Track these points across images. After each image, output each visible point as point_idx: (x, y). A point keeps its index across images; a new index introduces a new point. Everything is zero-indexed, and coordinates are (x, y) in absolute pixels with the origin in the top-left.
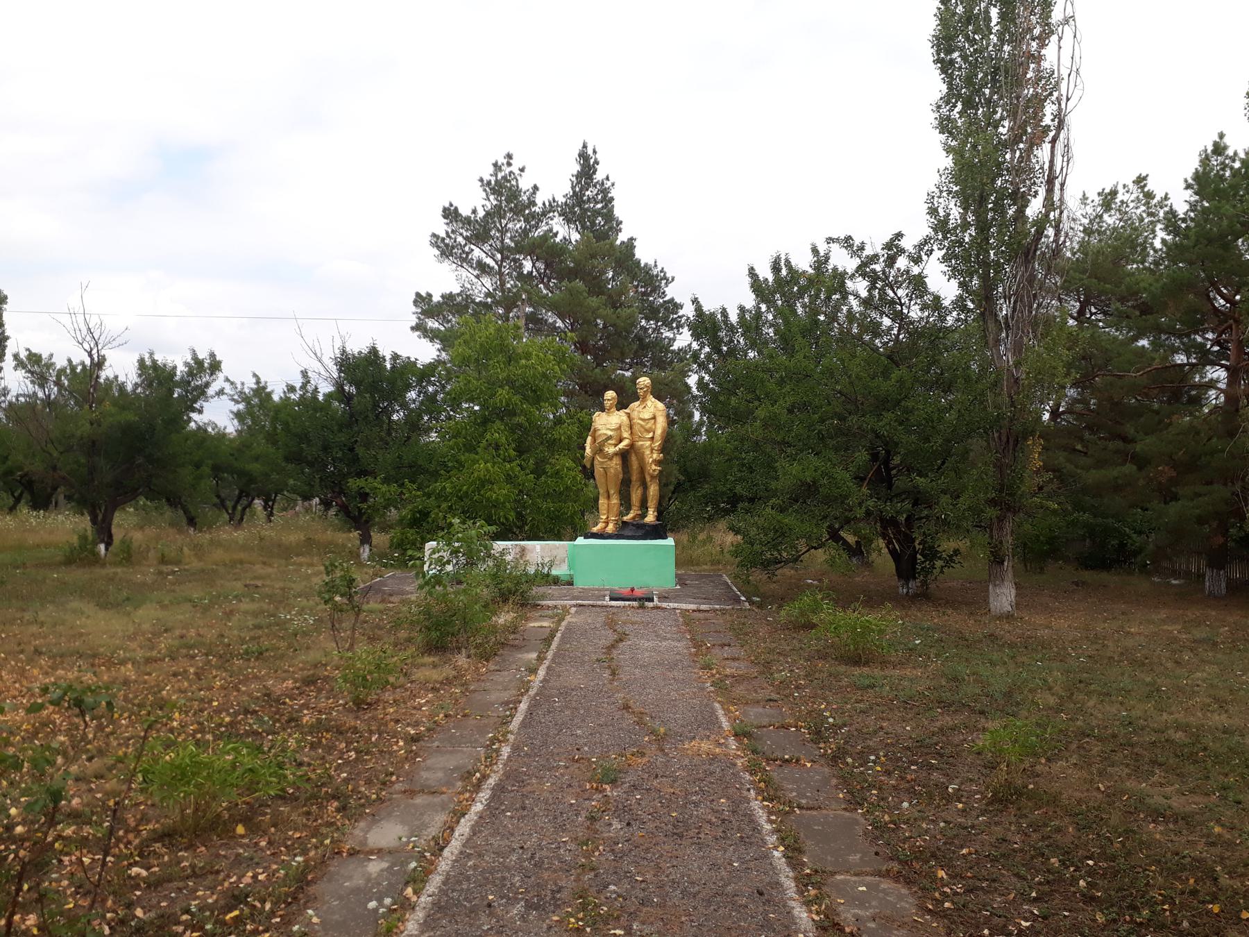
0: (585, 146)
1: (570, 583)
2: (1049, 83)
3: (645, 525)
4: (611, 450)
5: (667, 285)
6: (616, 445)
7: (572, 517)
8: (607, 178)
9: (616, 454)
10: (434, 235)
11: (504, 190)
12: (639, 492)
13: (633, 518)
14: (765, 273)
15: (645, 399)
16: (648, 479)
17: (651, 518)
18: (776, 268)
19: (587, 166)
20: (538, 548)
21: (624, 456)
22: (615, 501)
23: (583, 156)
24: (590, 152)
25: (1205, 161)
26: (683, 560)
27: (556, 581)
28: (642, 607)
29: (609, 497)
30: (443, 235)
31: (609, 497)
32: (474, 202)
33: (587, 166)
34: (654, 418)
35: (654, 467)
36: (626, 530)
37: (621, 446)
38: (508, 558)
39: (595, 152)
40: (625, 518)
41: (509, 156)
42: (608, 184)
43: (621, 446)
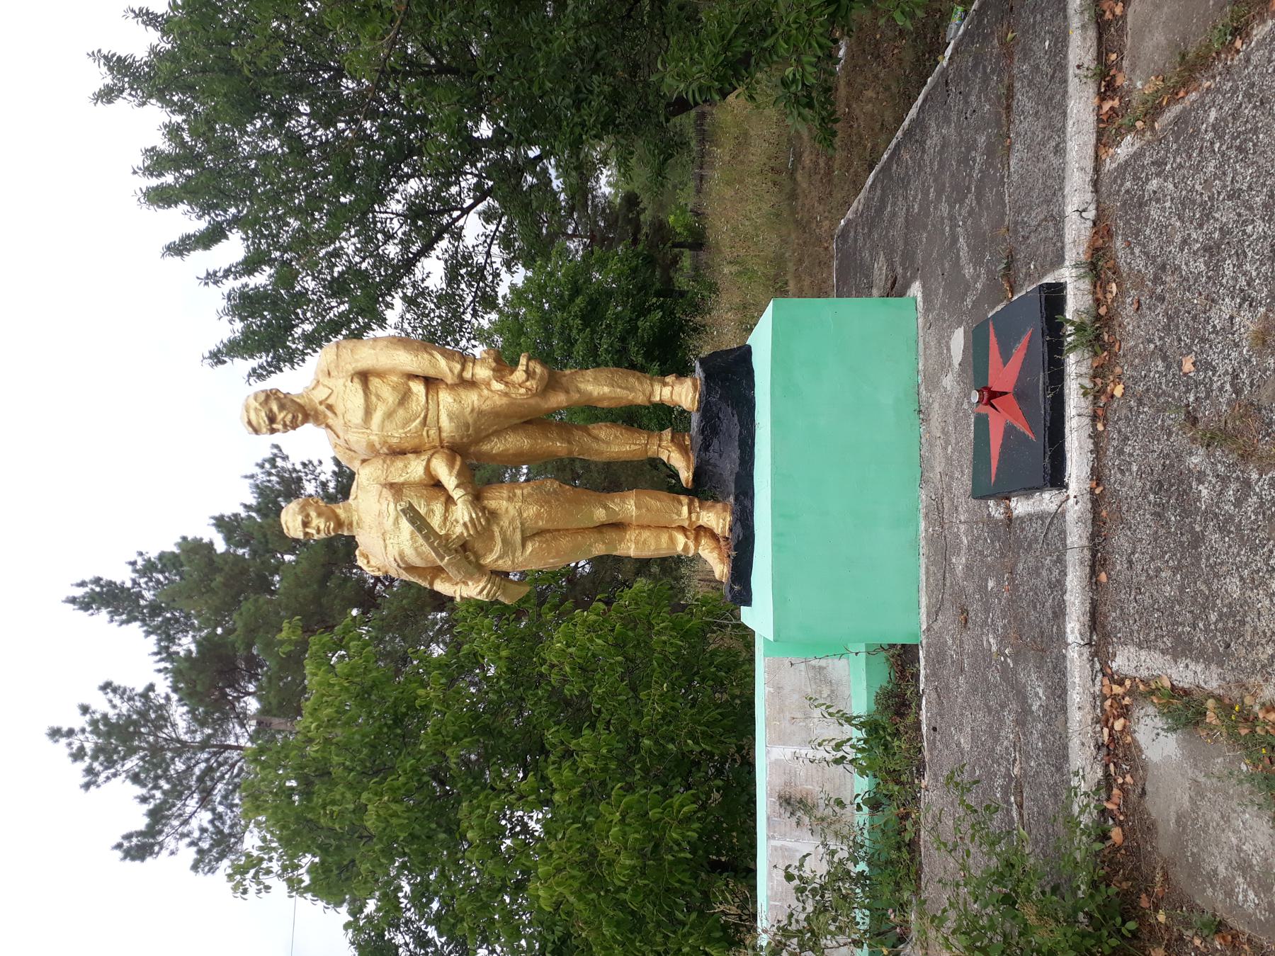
0: (73, 600)
1: (902, 658)
3: (706, 408)
5: (285, 458)
6: (449, 500)
7: (685, 635)
8: (133, 563)
9: (477, 498)
10: (195, 867)
11: (120, 738)
12: (603, 432)
13: (684, 450)
16: (558, 399)
17: (682, 393)
19: (106, 597)
20: (783, 753)
21: (481, 474)
22: (628, 505)
23: (86, 604)
24: (80, 592)
26: (832, 269)
27: (897, 703)
28: (1098, 334)
29: (619, 526)
30: (191, 854)
31: (619, 526)
32: (123, 803)
33: (106, 597)
34: (364, 377)
35: (519, 375)
36: (723, 475)
37: (449, 480)
38: (818, 868)
39: (83, 584)
40: (685, 475)
41: (55, 733)
42: (140, 562)
43: (449, 480)
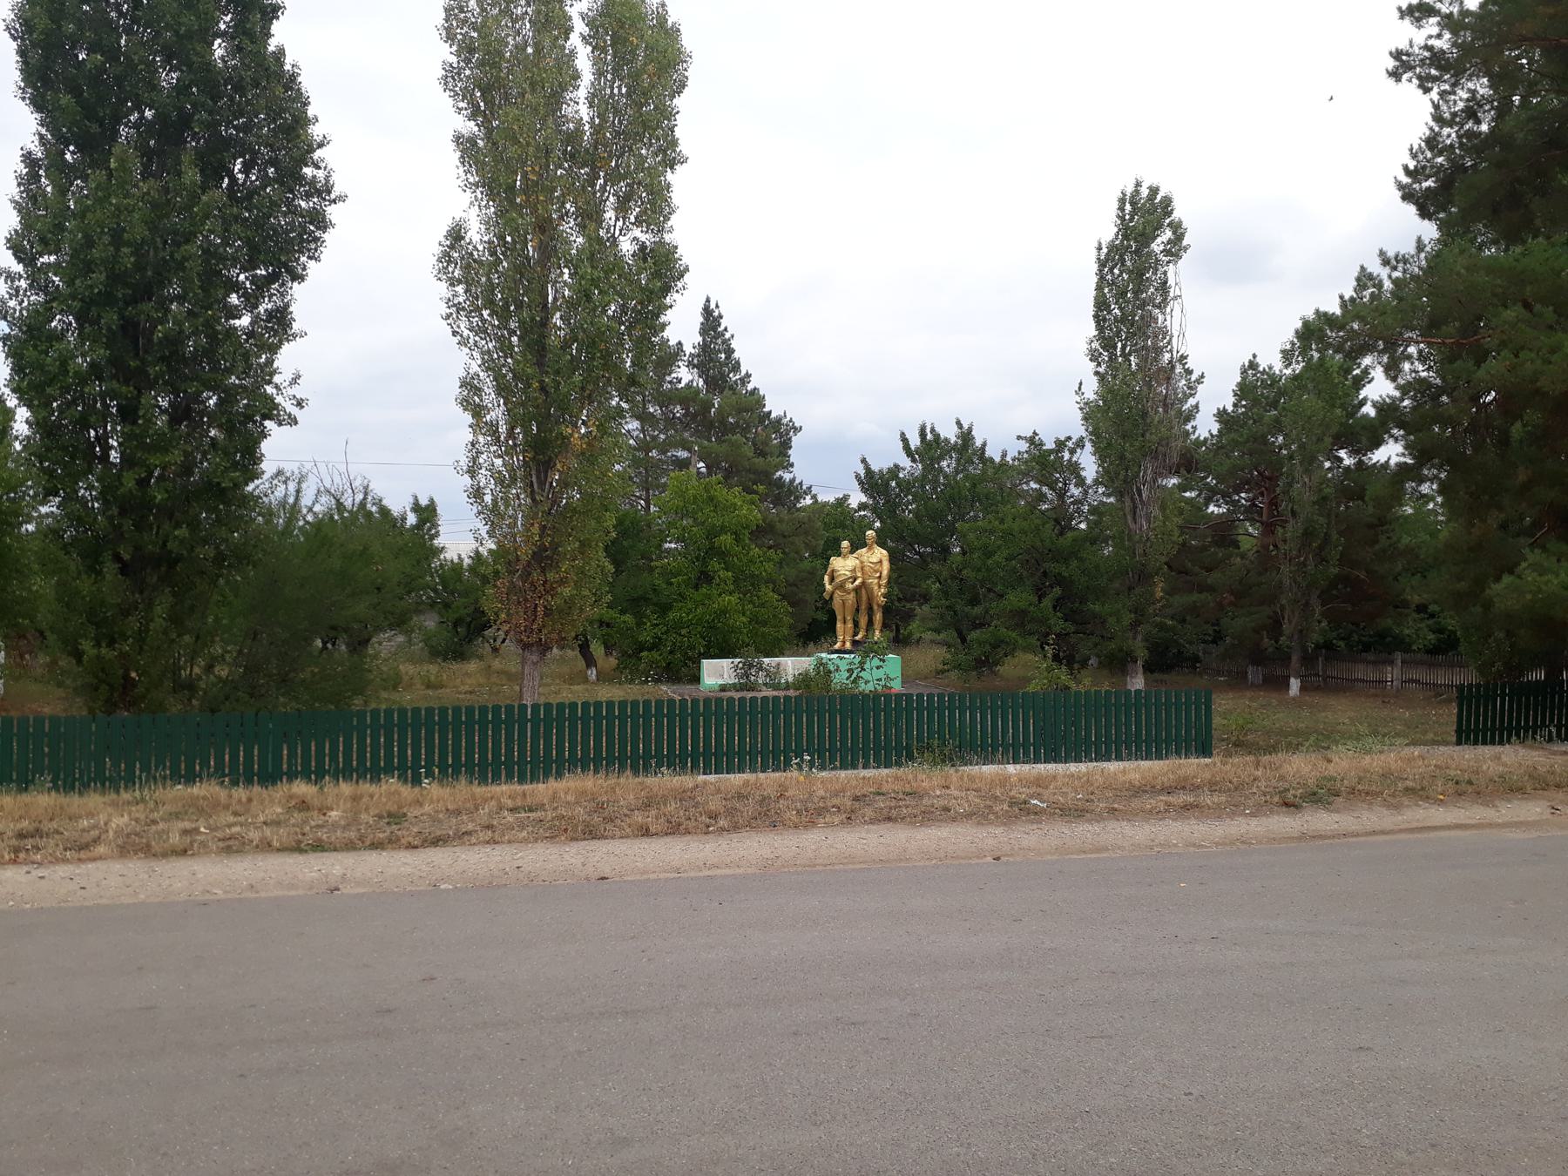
0: (708, 300)
2: (1164, 332)
4: (850, 586)
14: (915, 442)
15: (871, 548)
18: (923, 434)
21: (857, 590)
22: (850, 625)
24: (713, 306)
25: (1244, 372)
